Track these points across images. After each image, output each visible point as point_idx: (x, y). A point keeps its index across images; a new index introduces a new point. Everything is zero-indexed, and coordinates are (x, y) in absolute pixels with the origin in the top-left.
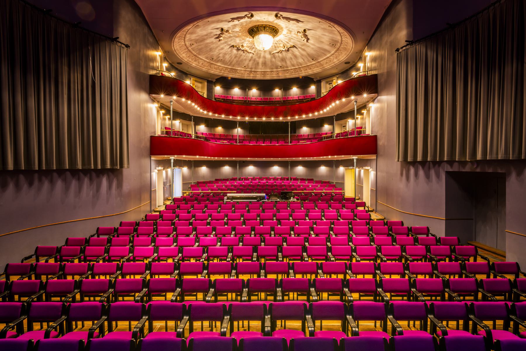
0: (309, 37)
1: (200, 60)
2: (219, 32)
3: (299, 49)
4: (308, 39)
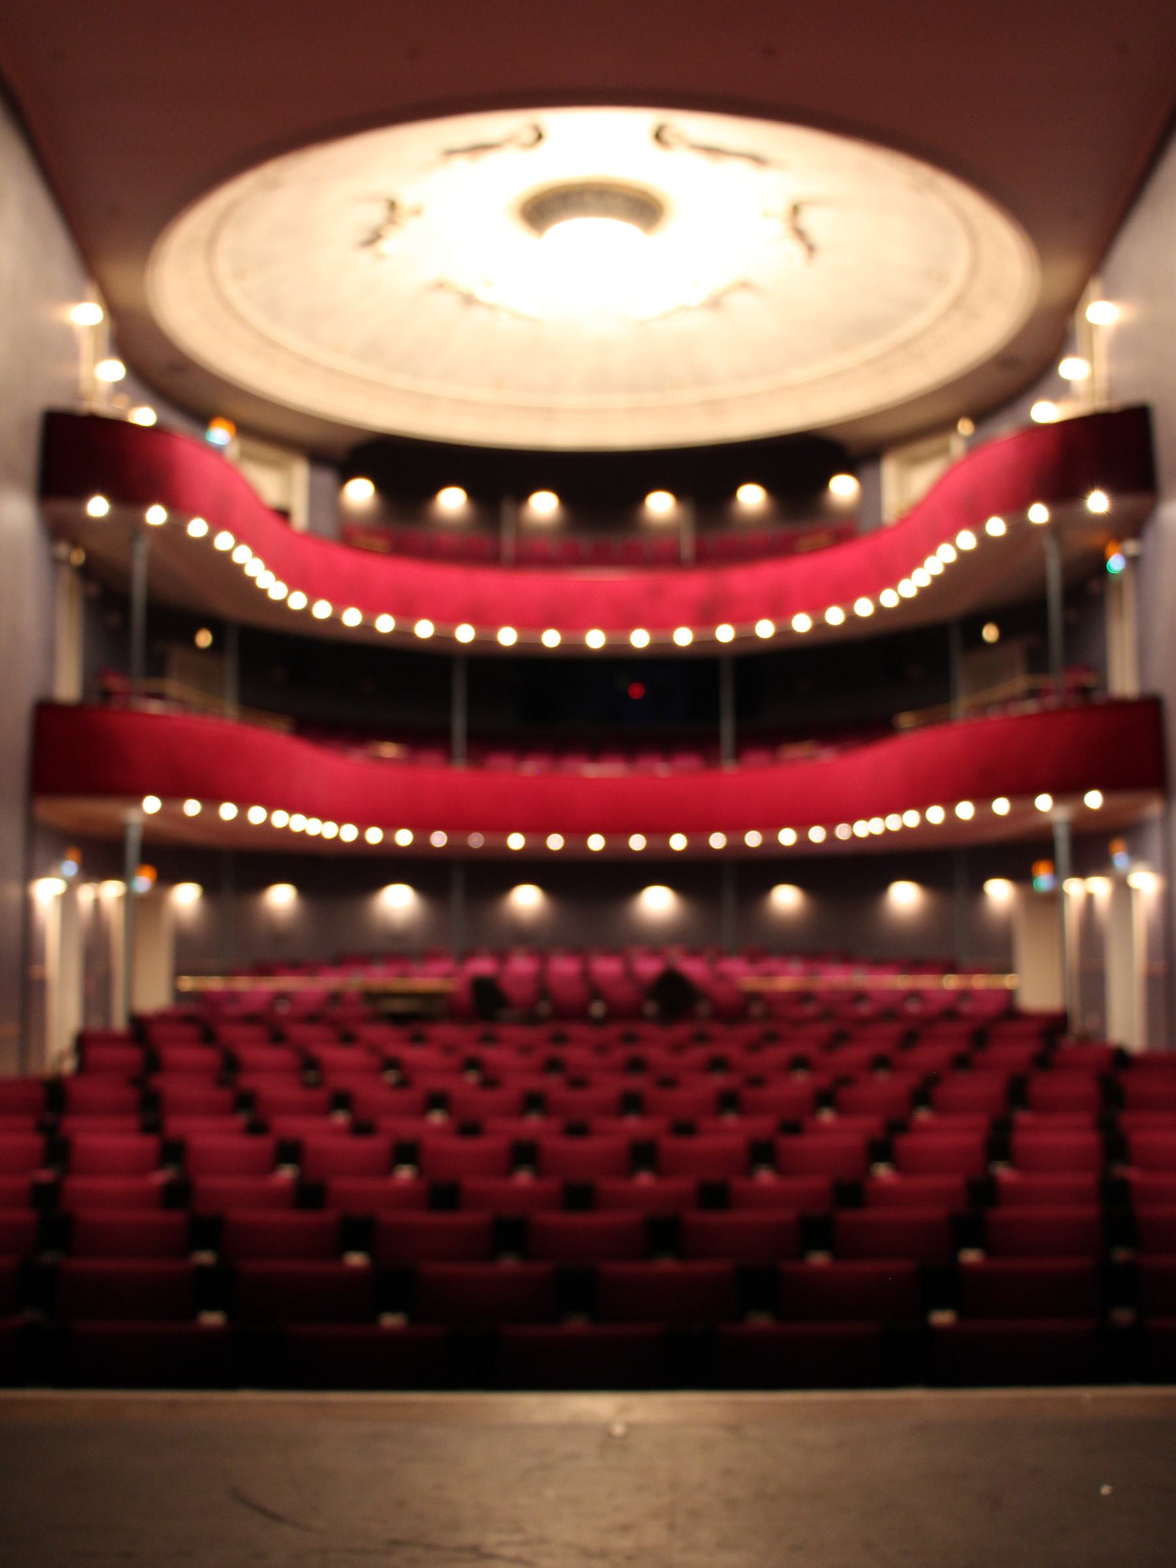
2: (376, 214)
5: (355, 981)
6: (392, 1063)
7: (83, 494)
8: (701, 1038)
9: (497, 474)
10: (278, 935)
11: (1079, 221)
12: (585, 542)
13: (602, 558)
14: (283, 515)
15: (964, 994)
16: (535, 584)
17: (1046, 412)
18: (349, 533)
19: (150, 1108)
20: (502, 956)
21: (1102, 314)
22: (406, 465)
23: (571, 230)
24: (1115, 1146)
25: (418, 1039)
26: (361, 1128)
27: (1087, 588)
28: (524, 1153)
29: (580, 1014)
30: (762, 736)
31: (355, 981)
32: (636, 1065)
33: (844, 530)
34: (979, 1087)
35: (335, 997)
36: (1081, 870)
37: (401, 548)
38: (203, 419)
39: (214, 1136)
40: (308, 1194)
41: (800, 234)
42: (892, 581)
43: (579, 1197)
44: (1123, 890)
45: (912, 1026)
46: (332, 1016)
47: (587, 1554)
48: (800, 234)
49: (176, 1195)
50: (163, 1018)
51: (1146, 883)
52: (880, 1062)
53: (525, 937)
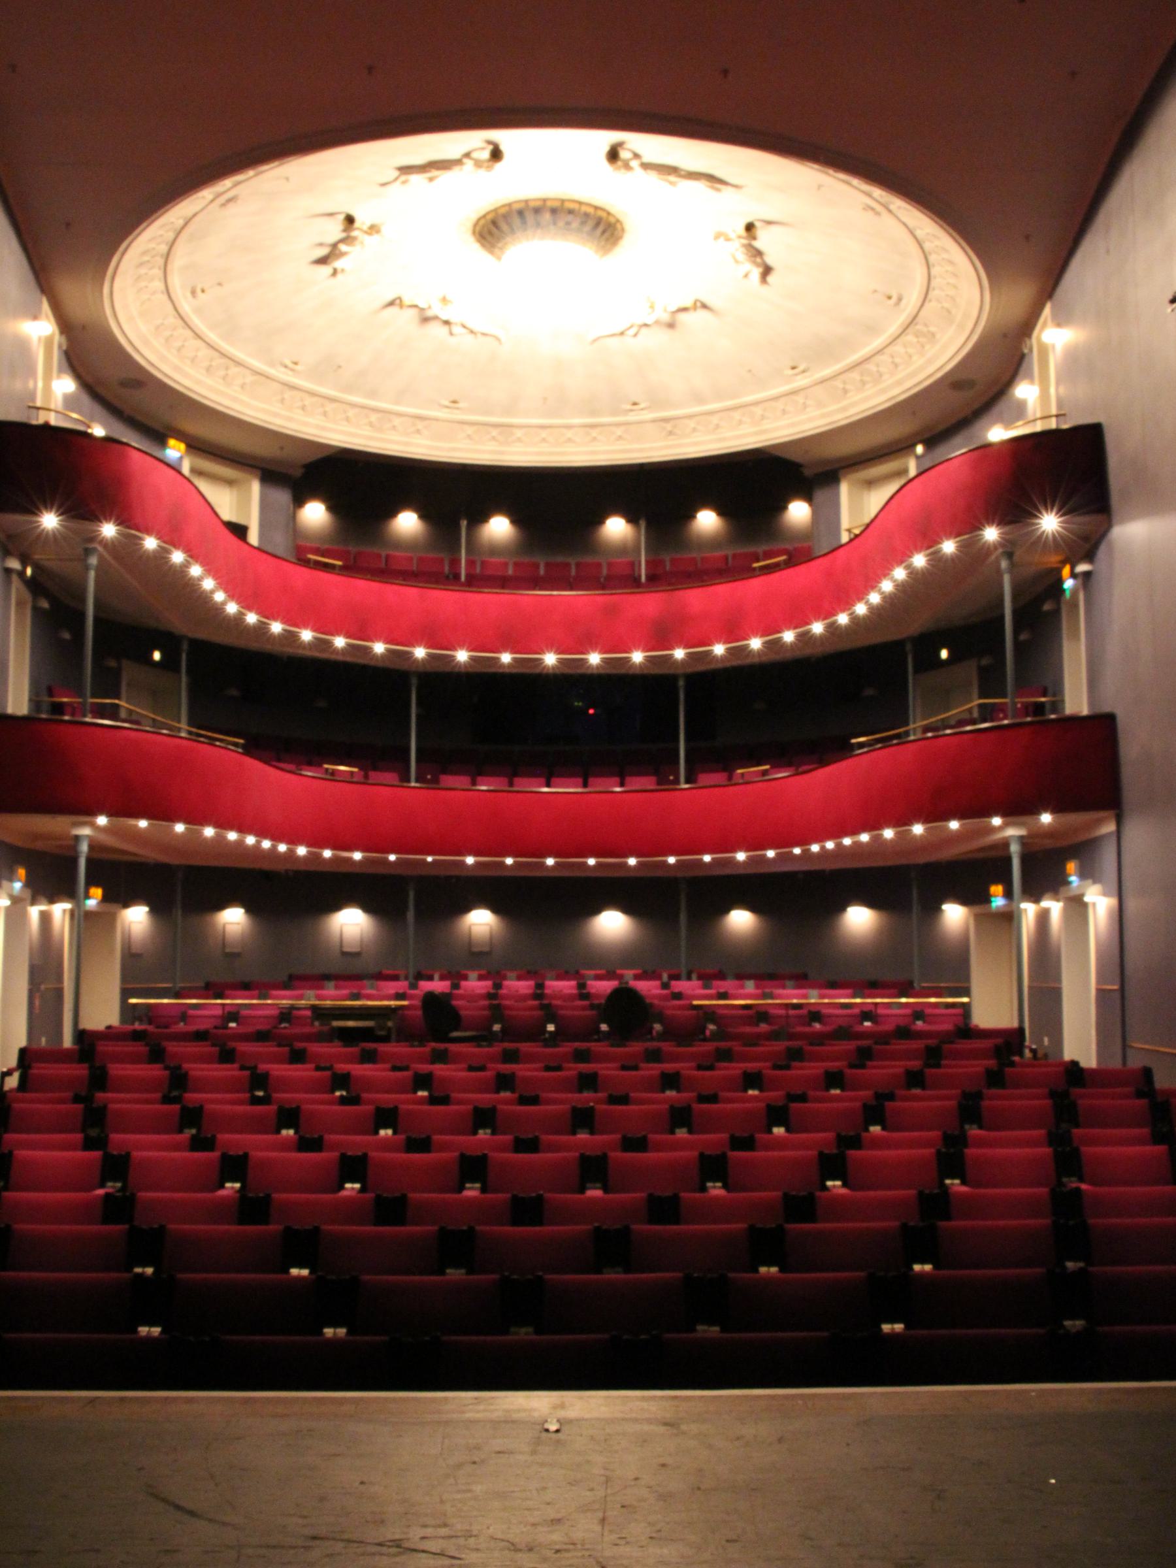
0: (769, 260)
1: (234, 370)
2: (333, 230)
3: (316, 1048)
4: (767, 271)
5: (308, 999)
6: (342, 1080)
7: (33, 510)
8: (654, 1056)
9: (451, 493)
10: (231, 955)
11: (1031, 212)
12: (541, 563)
13: (557, 579)
14: (239, 531)
15: (918, 1013)
16: (490, 603)
17: (997, 434)
18: (303, 552)
19: (94, 1123)
20: (456, 978)
21: (1055, 338)
22: (361, 484)
23: (530, 250)
24: (1068, 1160)
25: (369, 1057)
26: (306, 1144)
27: (1041, 607)
28: (473, 1167)
29: (535, 1033)
30: (716, 756)
31: (308, 999)
32: (588, 1081)
33: (799, 553)
34: (933, 1102)
35: (286, 1015)
36: (1034, 892)
37: (353, 568)
38: (160, 437)
39: (157, 1151)
40: (252, 1208)
41: (756, 254)
42: (846, 603)
43: (527, 1210)
44: (1077, 906)
45: (865, 1045)
46: (279, 1032)
47: (514, 1548)
48: (756, 254)
49: (118, 1209)
50: (110, 1034)
51: (1100, 903)
52: (834, 1079)
53: (478, 956)
